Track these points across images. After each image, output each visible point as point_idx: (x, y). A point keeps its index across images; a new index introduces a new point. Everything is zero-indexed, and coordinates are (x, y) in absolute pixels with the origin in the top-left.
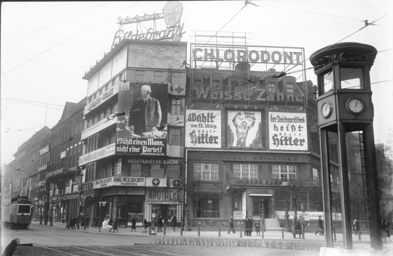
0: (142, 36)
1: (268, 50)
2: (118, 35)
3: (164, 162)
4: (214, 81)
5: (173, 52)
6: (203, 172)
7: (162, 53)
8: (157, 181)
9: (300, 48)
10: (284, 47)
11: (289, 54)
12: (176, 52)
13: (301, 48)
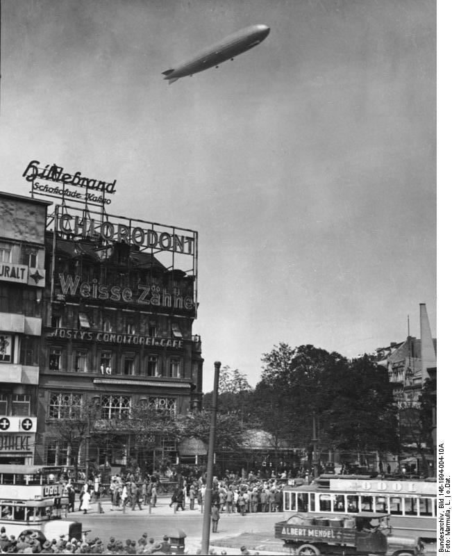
1: (156, 228)
5: (28, 214)
7: (12, 212)
8: (26, 426)
9: (171, 227)
10: (174, 228)
11: (180, 238)
12: (32, 213)
13: (194, 232)
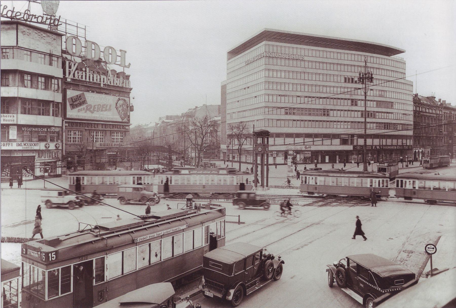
0: (19, 14)
2: (26, 12)
3: (49, 130)
4: (7, 55)
6: (73, 138)
12: (54, 39)
